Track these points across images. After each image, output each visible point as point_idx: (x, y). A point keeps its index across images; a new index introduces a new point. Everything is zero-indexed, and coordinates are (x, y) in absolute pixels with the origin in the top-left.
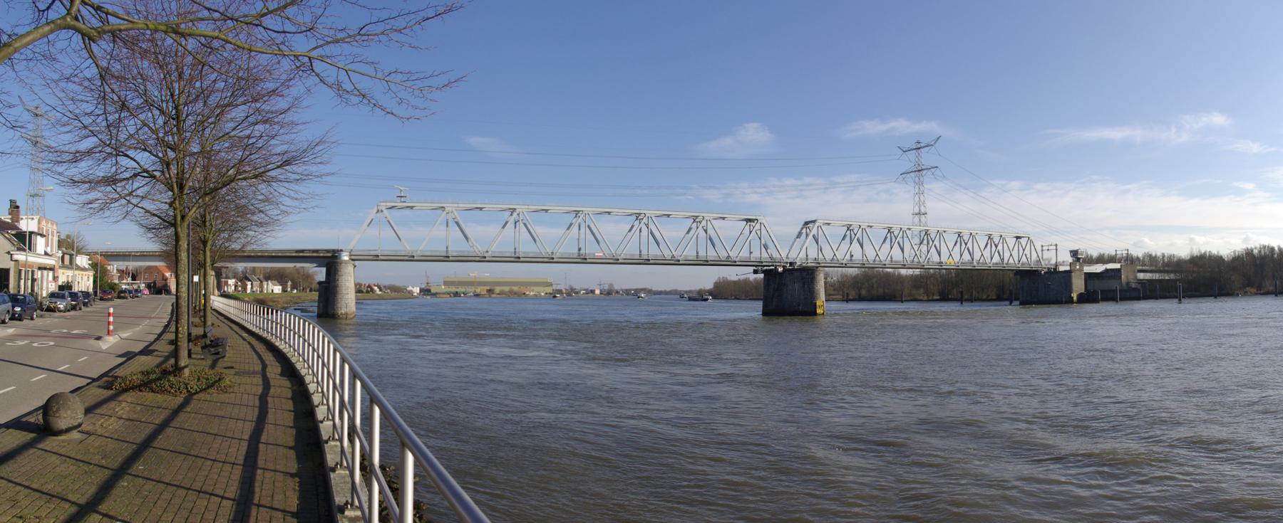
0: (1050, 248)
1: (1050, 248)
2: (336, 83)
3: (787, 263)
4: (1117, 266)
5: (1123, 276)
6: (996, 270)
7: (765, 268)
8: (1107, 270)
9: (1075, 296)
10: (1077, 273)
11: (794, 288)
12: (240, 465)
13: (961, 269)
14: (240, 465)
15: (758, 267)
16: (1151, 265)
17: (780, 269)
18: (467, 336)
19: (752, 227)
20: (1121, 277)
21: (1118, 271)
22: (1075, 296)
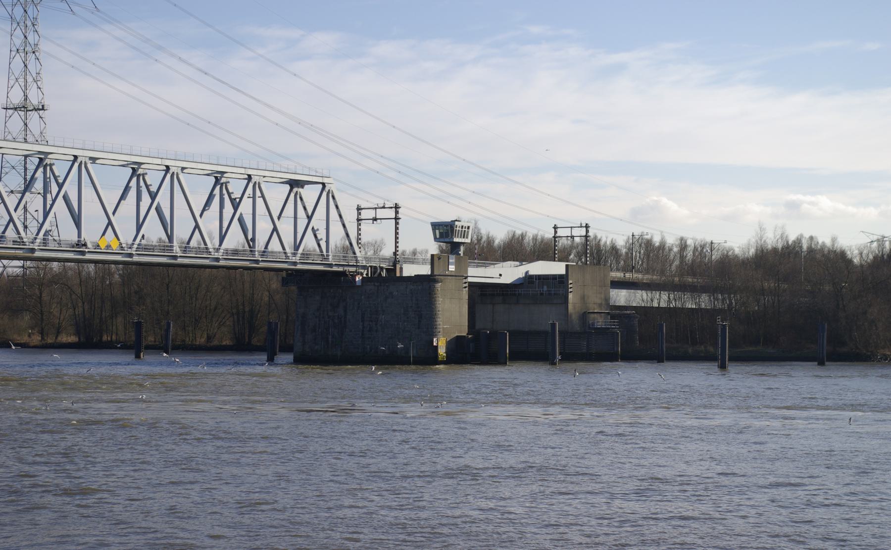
0: (381, 213)
1: (381, 213)
4: (557, 268)
5: (570, 296)
8: (529, 279)
9: (441, 345)
20: (567, 298)
21: (560, 281)
22: (441, 345)
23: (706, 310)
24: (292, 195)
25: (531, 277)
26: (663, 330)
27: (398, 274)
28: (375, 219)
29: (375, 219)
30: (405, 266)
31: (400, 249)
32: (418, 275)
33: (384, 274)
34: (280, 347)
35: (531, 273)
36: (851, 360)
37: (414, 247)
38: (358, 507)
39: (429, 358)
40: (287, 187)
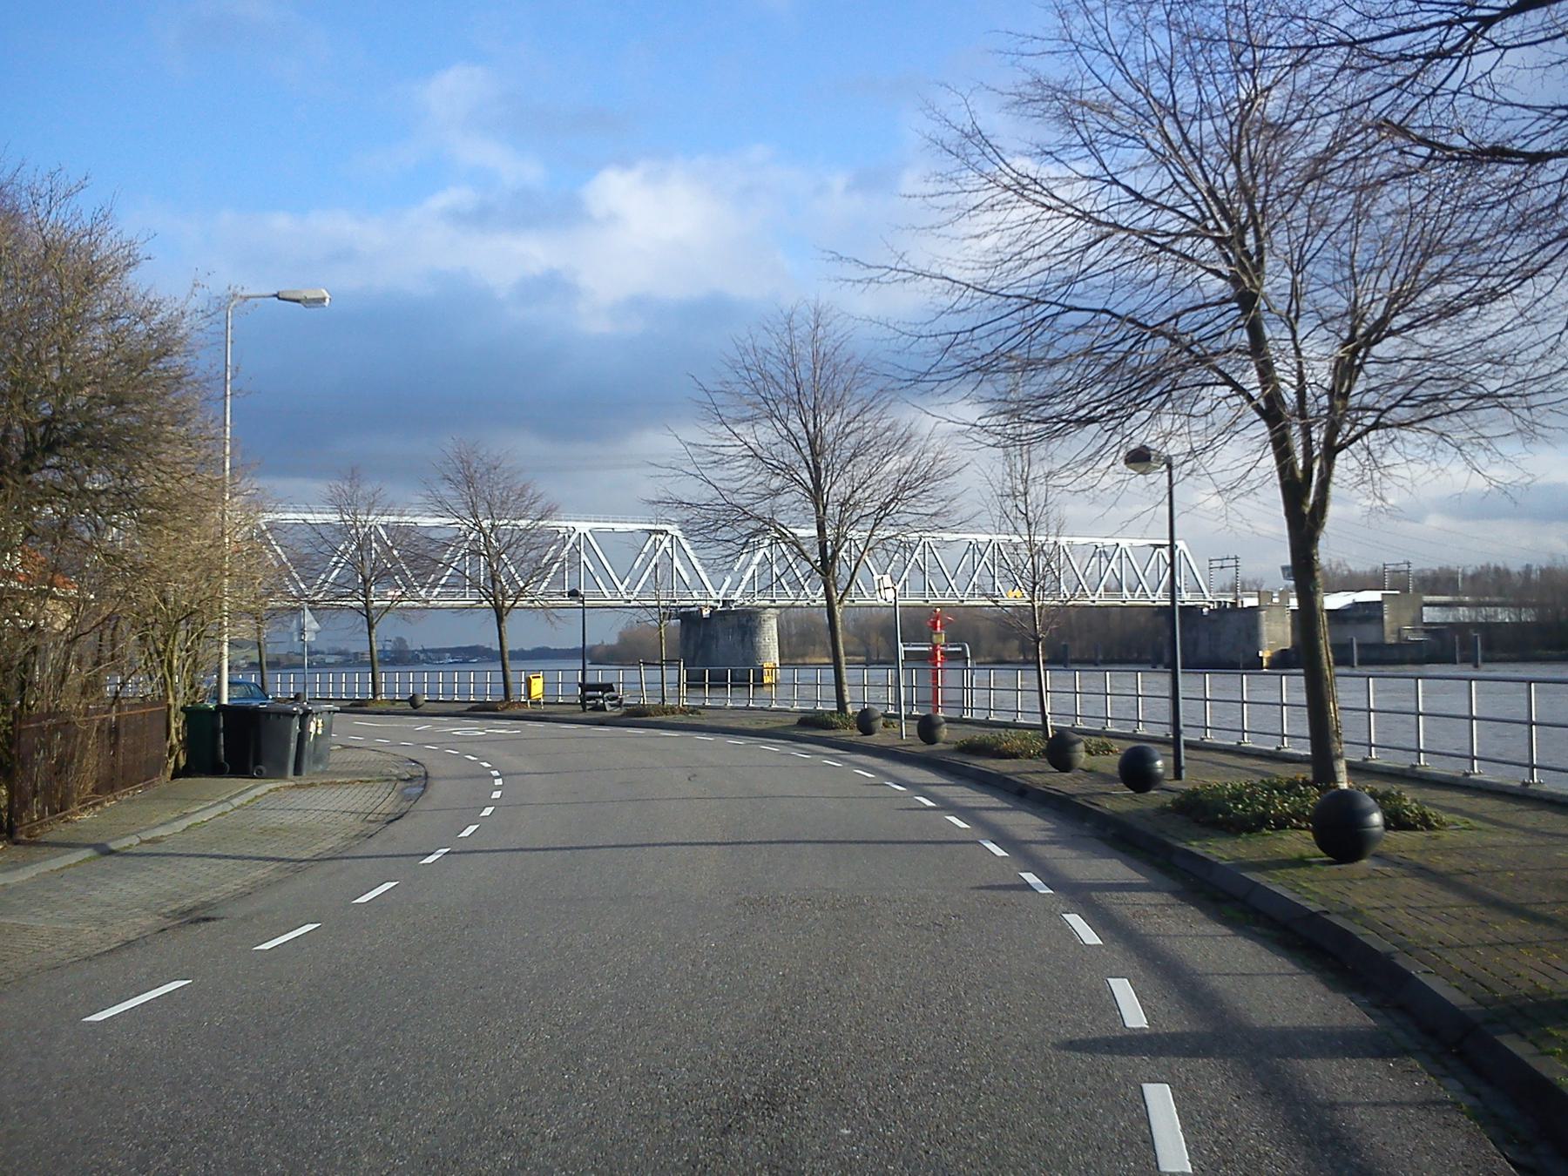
0: (1226, 563)
1: (1226, 563)
2: (1368, 487)
3: (718, 601)
4: (1375, 596)
5: (1386, 617)
6: (1106, 607)
7: (682, 610)
8: (1356, 604)
9: (1265, 654)
10: (1276, 612)
11: (726, 641)
12: (1166, 723)
13: (1159, 607)
14: (1166, 723)
15: (668, 613)
16: (1500, 594)
17: (706, 613)
18: (949, 660)
19: (658, 542)
20: (1382, 618)
21: (1378, 605)
22: (1265, 654)
23: (1481, 623)
24: (1156, 554)
25: (1357, 603)
26: (956, 652)
27: (1240, 606)
28: (1222, 567)
29: (1222, 567)
30: (1245, 600)
31: (587, 644)
32: (539, 649)
33: (1228, 605)
34: (1482, 657)
35: (1357, 600)
36: (532, 659)
37: (1525, 563)
38: (1207, 761)
39: (1255, 664)
40: (1152, 549)
